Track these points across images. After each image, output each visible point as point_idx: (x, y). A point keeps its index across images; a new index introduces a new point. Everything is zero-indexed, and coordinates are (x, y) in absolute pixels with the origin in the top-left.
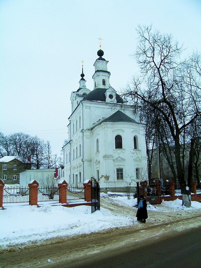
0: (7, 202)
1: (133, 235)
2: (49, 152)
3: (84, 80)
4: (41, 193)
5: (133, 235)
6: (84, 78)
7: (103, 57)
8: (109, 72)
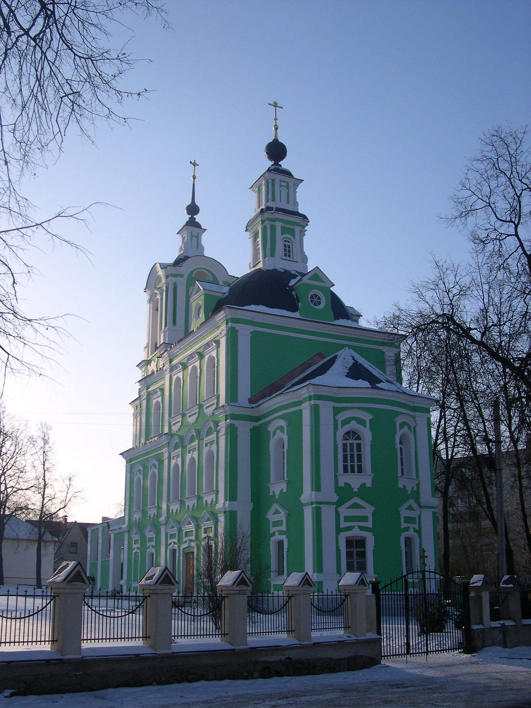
0: (137, 636)
1: (475, 656)
2: (44, 465)
3: (198, 225)
4: (186, 616)
5: (475, 656)
6: (198, 218)
7: (284, 164)
8: (304, 217)
